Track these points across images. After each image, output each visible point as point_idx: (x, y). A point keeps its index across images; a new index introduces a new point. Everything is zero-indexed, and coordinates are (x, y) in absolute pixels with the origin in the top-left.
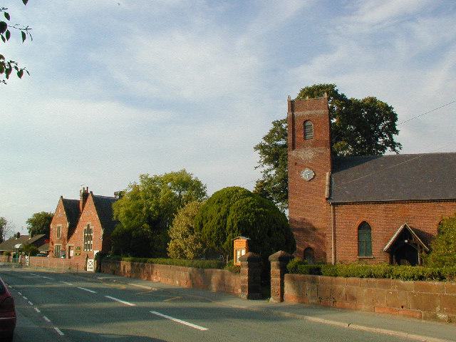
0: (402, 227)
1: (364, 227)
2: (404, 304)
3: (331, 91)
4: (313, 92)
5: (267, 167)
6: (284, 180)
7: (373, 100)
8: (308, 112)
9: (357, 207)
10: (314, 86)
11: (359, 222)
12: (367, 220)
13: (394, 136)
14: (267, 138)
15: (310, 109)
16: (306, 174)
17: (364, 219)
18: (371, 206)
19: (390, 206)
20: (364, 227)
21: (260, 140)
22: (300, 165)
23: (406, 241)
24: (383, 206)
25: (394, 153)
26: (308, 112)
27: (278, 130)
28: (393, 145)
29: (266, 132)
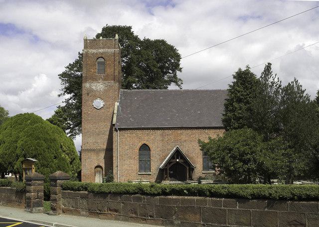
0: (175, 149)
1: (145, 148)
2: (151, 213)
3: (125, 32)
4: (109, 32)
5: (68, 96)
6: (79, 107)
7: (163, 42)
8: (101, 51)
9: (138, 132)
10: (119, 26)
11: (140, 144)
12: (147, 143)
13: (178, 73)
14: (71, 67)
15: (103, 48)
16: (99, 103)
17: (145, 142)
18: (152, 132)
19: (166, 131)
20: (145, 148)
21: (63, 70)
22: (95, 95)
23: (178, 160)
24: (159, 132)
25: (177, 88)
26: (101, 51)
27: (78, 65)
28: (175, 80)
29: (72, 61)
